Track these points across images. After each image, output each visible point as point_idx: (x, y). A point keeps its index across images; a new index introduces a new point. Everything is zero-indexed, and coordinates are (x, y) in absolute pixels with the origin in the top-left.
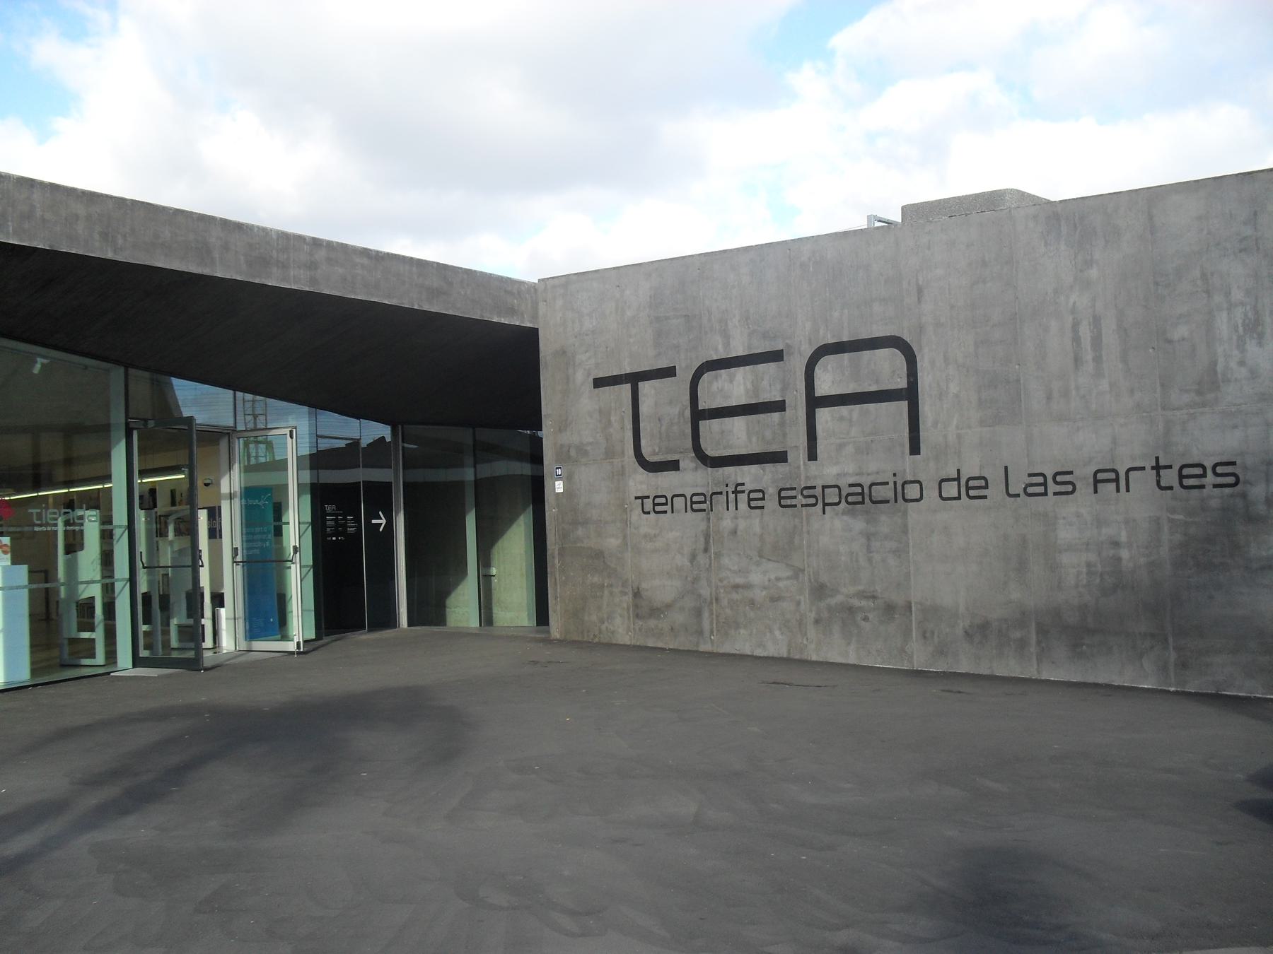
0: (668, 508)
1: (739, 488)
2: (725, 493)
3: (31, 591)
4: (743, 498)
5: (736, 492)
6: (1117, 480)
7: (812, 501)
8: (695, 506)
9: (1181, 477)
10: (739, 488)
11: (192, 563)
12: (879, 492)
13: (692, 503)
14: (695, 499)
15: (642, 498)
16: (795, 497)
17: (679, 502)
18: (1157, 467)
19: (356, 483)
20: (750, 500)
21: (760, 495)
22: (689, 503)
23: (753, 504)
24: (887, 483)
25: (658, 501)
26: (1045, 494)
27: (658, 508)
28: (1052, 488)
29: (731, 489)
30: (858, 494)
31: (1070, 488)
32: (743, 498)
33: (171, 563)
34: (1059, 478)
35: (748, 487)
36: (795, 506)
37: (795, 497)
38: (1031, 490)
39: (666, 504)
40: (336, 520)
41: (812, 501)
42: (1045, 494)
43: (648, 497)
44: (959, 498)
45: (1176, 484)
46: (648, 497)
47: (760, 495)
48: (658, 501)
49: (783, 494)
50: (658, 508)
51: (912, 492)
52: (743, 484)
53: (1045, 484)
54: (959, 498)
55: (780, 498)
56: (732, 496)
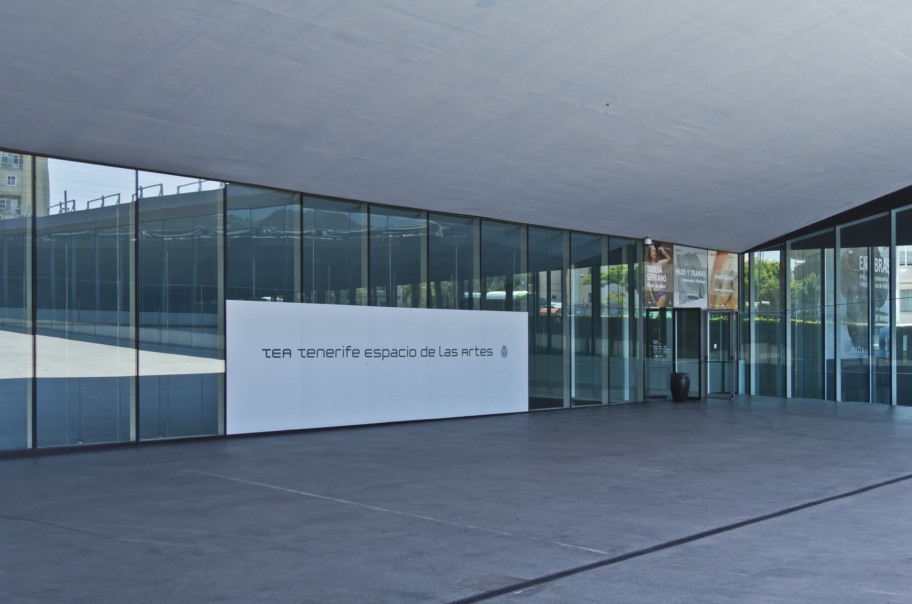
0: (315, 355)
1: (349, 348)
2: (342, 350)
3: (203, 313)
4: (350, 353)
5: (347, 350)
6: (467, 353)
7: (379, 355)
8: (328, 355)
9: (273, 353)
10: (349, 348)
11: (16, 199)
12: (402, 353)
13: (327, 353)
14: (328, 351)
15: (266, 350)
16: (371, 353)
17: (321, 353)
18: (476, 349)
19: (562, 331)
20: (353, 353)
21: (358, 352)
22: (398, 353)
23: (354, 355)
24: (341, 350)
25: (482, 351)
26: (450, 356)
27: (482, 354)
28: (452, 354)
29: (345, 348)
30: (310, 353)
31: (491, 354)
32: (350, 353)
33: (298, 204)
34: (453, 351)
35: (352, 348)
36: (371, 357)
37: (371, 353)
38: (446, 354)
39: (314, 353)
40: (658, 348)
41: (379, 355)
42: (450, 356)
43: (270, 350)
44: (427, 356)
45: (306, 356)
46: (270, 350)
47: (358, 352)
48: (482, 351)
49: (367, 352)
50: (482, 354)
51: (424, 353)
52: (350, 347)
53: (450, 353)
54: (427, 356)
55: (366, 353)
56: (345, 352)
